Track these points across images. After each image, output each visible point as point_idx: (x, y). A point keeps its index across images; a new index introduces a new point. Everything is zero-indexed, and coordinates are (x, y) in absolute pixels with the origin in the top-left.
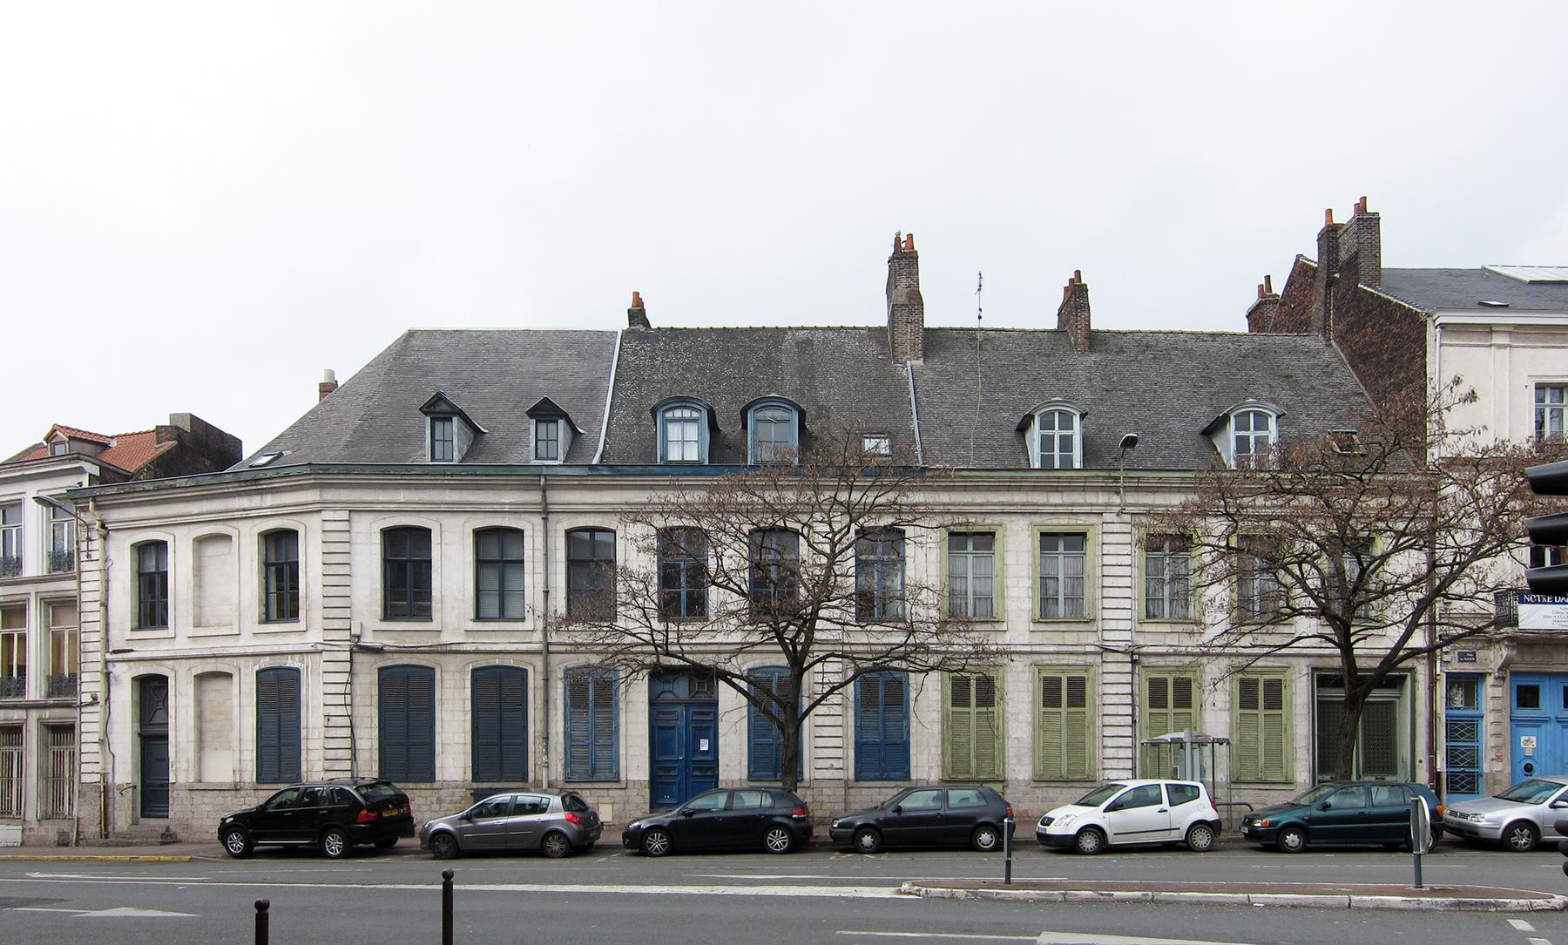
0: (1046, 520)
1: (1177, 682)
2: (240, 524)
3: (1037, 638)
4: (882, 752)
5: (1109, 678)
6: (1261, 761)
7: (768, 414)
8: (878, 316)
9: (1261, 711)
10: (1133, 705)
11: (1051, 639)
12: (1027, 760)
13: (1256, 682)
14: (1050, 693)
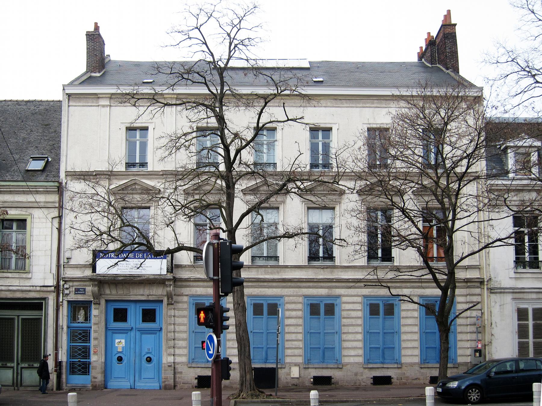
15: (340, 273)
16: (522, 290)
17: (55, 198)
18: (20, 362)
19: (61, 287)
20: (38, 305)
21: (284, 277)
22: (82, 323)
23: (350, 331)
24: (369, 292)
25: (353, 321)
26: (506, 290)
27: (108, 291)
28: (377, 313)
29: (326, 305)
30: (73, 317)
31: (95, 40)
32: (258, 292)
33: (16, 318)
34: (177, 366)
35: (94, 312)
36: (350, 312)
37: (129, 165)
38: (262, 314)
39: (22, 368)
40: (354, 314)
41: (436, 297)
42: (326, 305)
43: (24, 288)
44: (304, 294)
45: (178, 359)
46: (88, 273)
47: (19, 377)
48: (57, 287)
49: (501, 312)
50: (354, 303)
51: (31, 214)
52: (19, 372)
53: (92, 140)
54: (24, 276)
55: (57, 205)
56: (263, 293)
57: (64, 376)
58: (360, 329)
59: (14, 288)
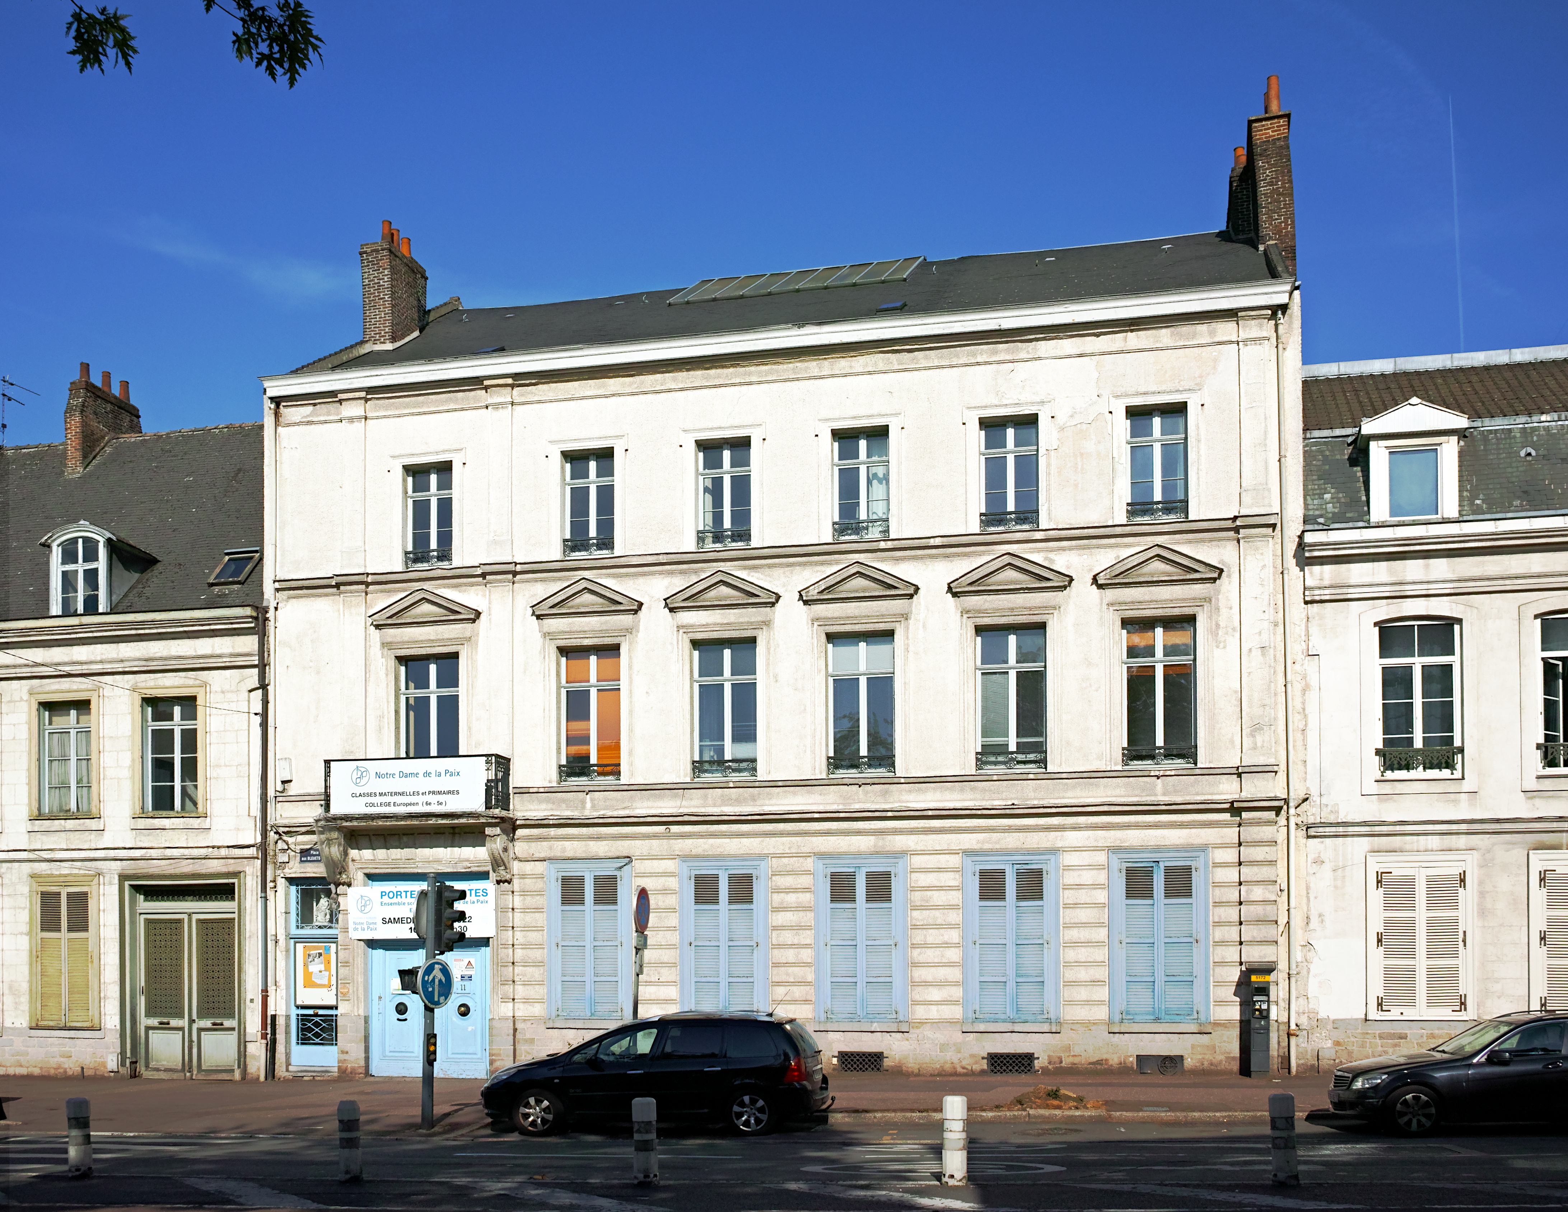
15: (905, 797)
16: (1398, 828)
18: (195, 1017)
19: (272, 847)
21: (767, 809)
22: (320, 927)
23: (930, 940)
24: (978, 842)
25: (939, 916)
26: (1350, 829)
28: (1000, 895)
29: (871, 877)
32: (706, 847)
33: (186, 917)
34: (519, 1026)
36: (929, 893)
38: (582, 902)
39: (200, 1030)
40: (939, 898)
42: (871, 877)
43: (196, 853)
44: (816, 850)
45: (522, 1011)
47: (195, 1051)
48: (263, 847)
49: (1336, 887)
50: (939, 870)
51: (204, 685)
52: (195, 1038)
54: (195, 823)
55: (255, 660)
56: (718, 851)
57: (280, 1048)
58: (954, 936)
59: (176, 853)
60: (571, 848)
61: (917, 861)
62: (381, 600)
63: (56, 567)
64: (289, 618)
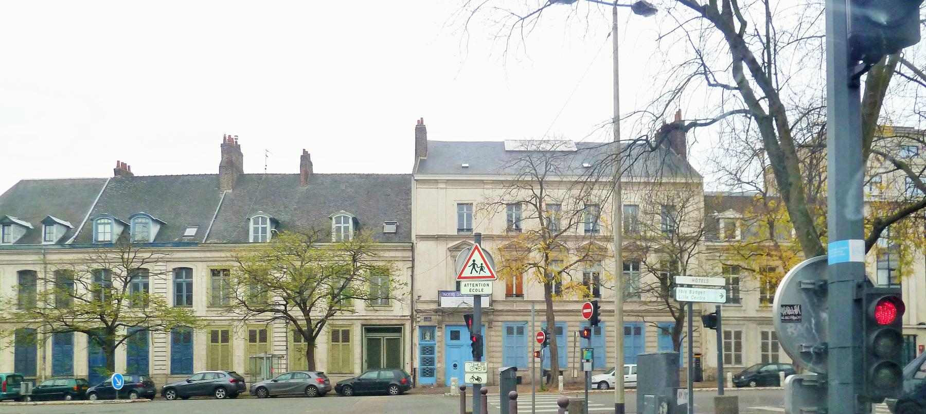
0: (213, 264)
1: (736, 332)
2: (197, 264)
3: (210, 314)
4: (182, 360)
5: (277, 330)
6: (341, 364)
7: (140, 220)
8: (297, 171)
9: (341, 343)
10: (287, 341)
11: (213, 315)
12: (242, 365)
13: (730, 332)
14: (214, 337)
17: (409, 254)
20: (398, 329)
27: (447, 319)
30: (423, 337)
31: (421, 130)
35: (438, 333)
37: (459, 230)
41: (671, 322)
46: (434, 306)
48: (412, 316)
53: (432, 210)
60: (510, 318)
61: (608, 324)
62: (452, 244)
63: (252, 226)
64: (421, 247)
